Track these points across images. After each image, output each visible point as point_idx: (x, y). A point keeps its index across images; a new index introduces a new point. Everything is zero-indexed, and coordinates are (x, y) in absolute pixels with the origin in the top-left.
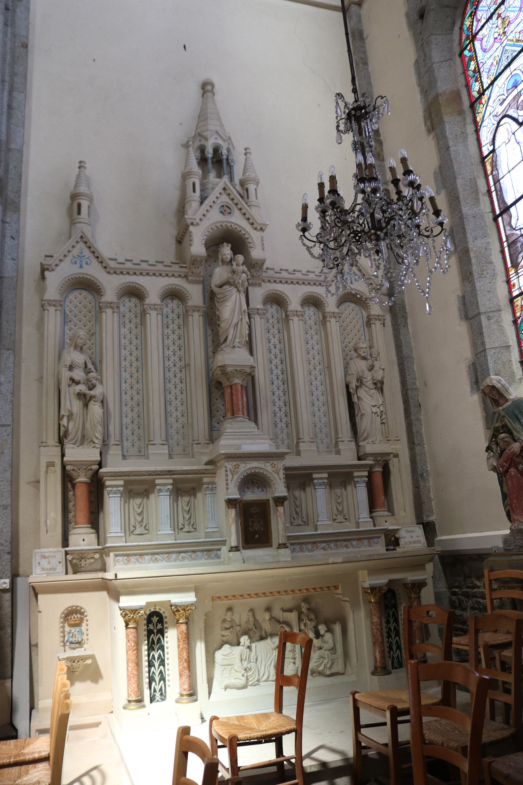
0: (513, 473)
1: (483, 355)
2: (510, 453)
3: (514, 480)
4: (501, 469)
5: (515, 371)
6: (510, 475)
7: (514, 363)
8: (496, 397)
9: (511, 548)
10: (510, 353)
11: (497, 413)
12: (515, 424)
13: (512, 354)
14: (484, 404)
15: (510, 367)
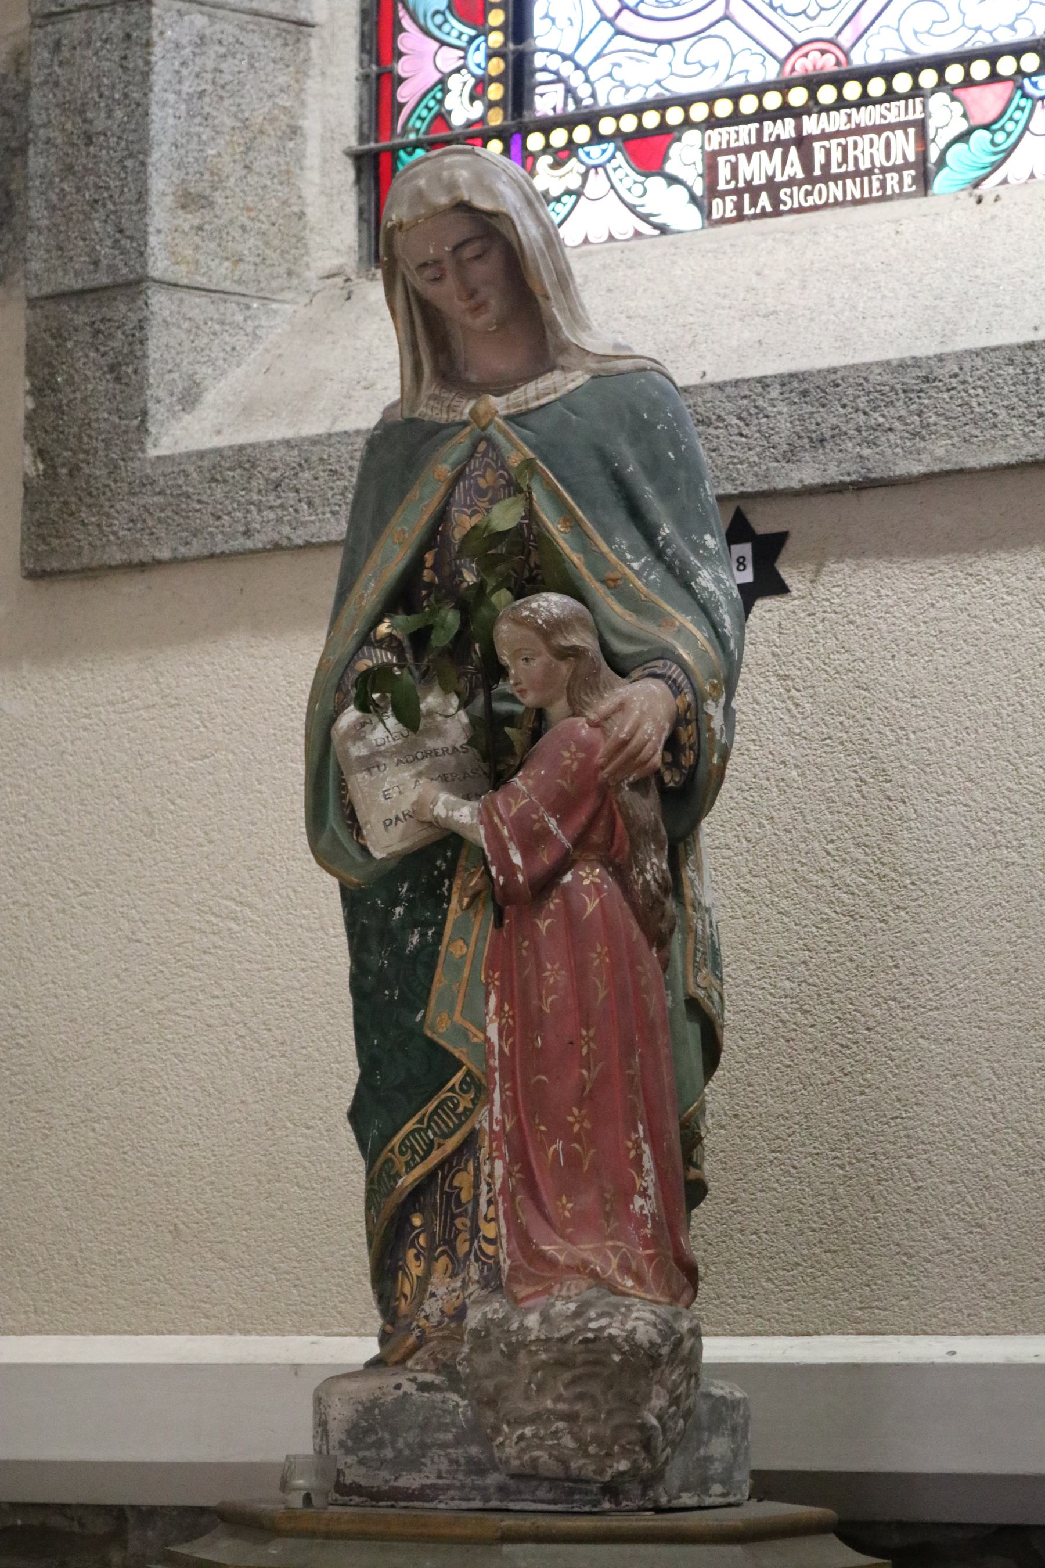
0: (591, 906)
1: (115, 28)
2: (602, 750)
3: (597, 957)
4: (517, 859)
5: (314, 213)
6: (571, 916)
7: (313, 149)
8: (477, 309)
9: (411, 1481)
10: (301, 72)
11: (463, 441)
12: (609, 541)
13: (313, 85)
14: (36, 392)
15: (287, 177)
